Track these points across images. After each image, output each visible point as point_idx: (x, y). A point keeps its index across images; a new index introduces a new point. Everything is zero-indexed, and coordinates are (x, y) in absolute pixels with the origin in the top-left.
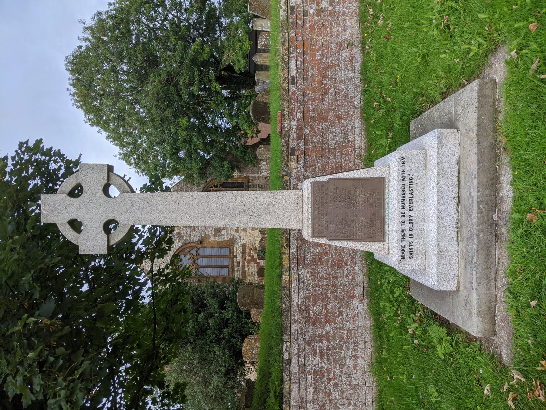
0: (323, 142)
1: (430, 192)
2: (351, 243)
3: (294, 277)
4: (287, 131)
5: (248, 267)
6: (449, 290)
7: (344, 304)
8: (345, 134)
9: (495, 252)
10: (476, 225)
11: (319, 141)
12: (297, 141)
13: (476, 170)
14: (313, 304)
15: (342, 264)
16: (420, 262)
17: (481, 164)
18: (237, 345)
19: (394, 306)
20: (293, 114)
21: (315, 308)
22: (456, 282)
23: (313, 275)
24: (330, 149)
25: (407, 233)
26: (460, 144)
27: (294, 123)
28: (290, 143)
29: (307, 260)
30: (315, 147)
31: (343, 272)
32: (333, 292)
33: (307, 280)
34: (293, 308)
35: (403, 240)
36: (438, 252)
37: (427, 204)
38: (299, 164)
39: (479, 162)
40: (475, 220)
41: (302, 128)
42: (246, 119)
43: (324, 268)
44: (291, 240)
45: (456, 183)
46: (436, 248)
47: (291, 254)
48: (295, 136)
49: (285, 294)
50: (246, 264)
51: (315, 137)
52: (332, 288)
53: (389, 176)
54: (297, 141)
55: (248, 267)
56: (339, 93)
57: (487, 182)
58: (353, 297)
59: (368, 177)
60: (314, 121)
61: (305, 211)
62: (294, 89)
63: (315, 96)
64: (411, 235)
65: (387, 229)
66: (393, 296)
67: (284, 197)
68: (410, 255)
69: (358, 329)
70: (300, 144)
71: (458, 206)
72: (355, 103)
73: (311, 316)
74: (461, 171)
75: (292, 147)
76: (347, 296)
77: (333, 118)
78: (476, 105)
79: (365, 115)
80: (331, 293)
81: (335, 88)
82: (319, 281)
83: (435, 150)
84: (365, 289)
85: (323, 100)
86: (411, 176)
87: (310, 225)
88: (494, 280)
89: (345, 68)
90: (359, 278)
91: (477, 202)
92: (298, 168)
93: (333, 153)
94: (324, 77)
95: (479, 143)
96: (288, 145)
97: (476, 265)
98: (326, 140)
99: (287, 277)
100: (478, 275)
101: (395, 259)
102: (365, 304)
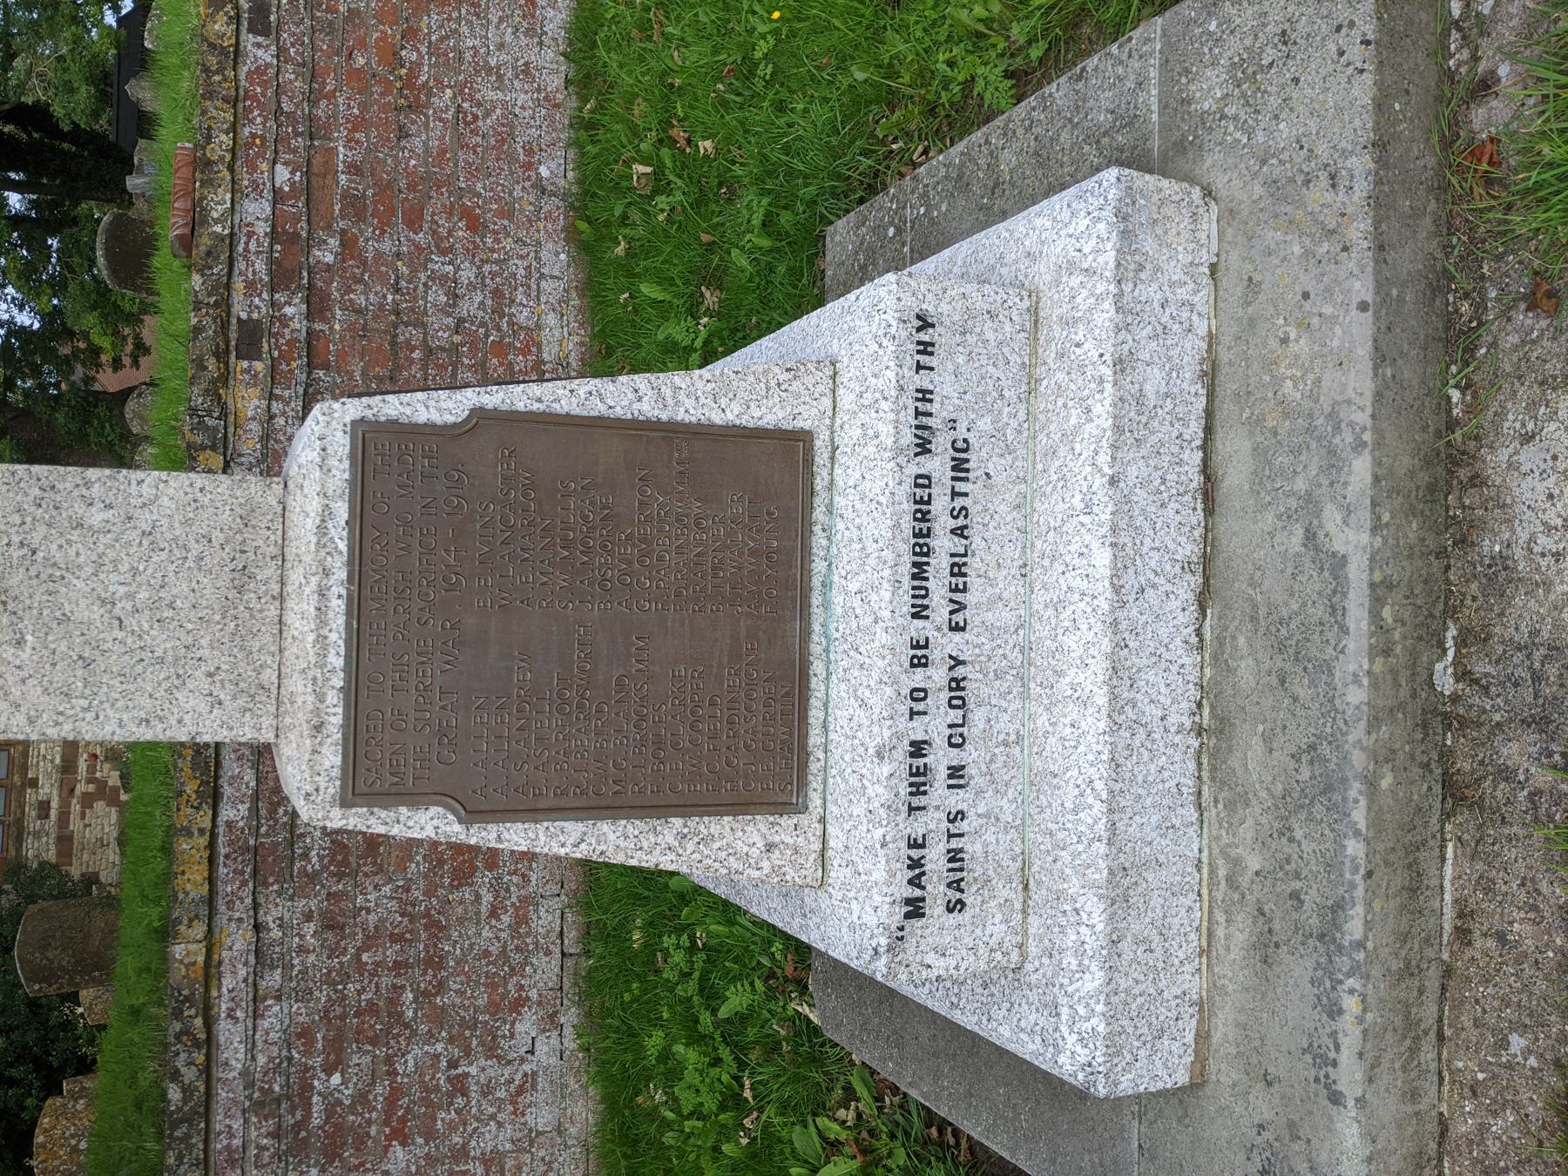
0: (398, 314)
1: (1067, 527)
2: (605, 827)
3: (236, 941)
4: (219, 238)
5: (83, 816)
6: (1160, 1086)
7: (475, 1042)
8: (497, 293)
9: (1442, 877)
10: (1362, 725)
11: (381, 307)
12: (273, 291)
13: (1367, 402)
14: (326, 1060)
15: (471, 861)
16: (997, 929)
17: (1389, 372)
18: (23, 1108)
19: (717, 1062)
20: (253, 168)
21: (336, 1079)
22: (1190, 1038)
23: (331, 924)
24: (429, 352)
25: (940, 759)
26: (1213, 268)
27: (257, 210)
28: (238, 298)
29: (305, 856)
30: (359, 332)
31: (478, 897)
32: (426, 994)
33: (302, 950)
34: (222, 1094)
35: (916, 802)
36: (1111, 872)
37: (1040, 597)
38: (278, 398)
39: (1380, 357)
40: (1356, 696)
41: (296, 235)
42: (93, 296)
43: (387, 889)
44: (226, 763)
45: (1197, 480)
46: (1101, 848)
47: (221, 830)
48: (260, 266)
49: (187, 1031)
50: (76, 807)
51: (360, 288)
52: (425, 973)
53: (831, 427)
54: (273, 291)
55: (83, 816)
56: (476, 118)
57: (1411, 474)
58: (518, 1004)
59: (717, 418)
60: (360, 217)
61: (300, 622)
62: (266, 56)
63: (364, 107)
64: (956, 772)
65: (815, 738)
66: (714, 1012)
67: (144, 520)
68: (950, 893)
69: (531, 1145)
70: (289, 310)
71: (1202, 609)
72: (544, 171)
73: (316, 1120)
74: (1218, 416)
75: (244, 316)
76: (491, 1003)
77: (448, 220)
78: (1369, 29)
79: (583, 226)
80: (415, 1000)
81: (459, 91)
82: (359, 951)
83: (1101, 288)
84: (569, 963)
85: (403, 134)
86: (961, 432)
87: (335, 720)
88: (1432, 1035)
89: (501, 20)
90: (545, 920)
91: (1372, 585)
92: (272, 417)
93: (443, 367)
94: (410, 34)
95: (1381, 248)
96: (225, 304)
97: (1361, 956)
98: (412, 310)
99: (193, 947)
100: (1369, 1016)
101: (871, 919)
102: (568, 1030)
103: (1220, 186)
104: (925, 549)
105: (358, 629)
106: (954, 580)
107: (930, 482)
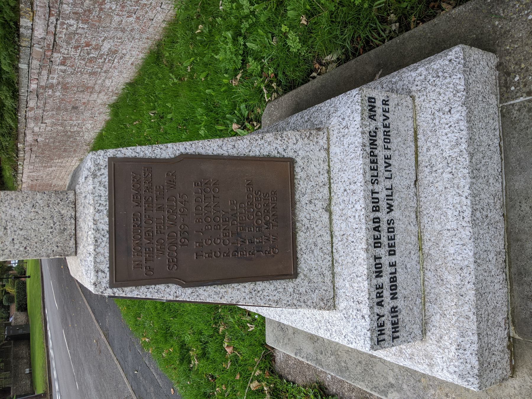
103: (514, 382)
104: (377, 208)
105: (150, 162)
106: (389, 234)
107: (375, 100)
